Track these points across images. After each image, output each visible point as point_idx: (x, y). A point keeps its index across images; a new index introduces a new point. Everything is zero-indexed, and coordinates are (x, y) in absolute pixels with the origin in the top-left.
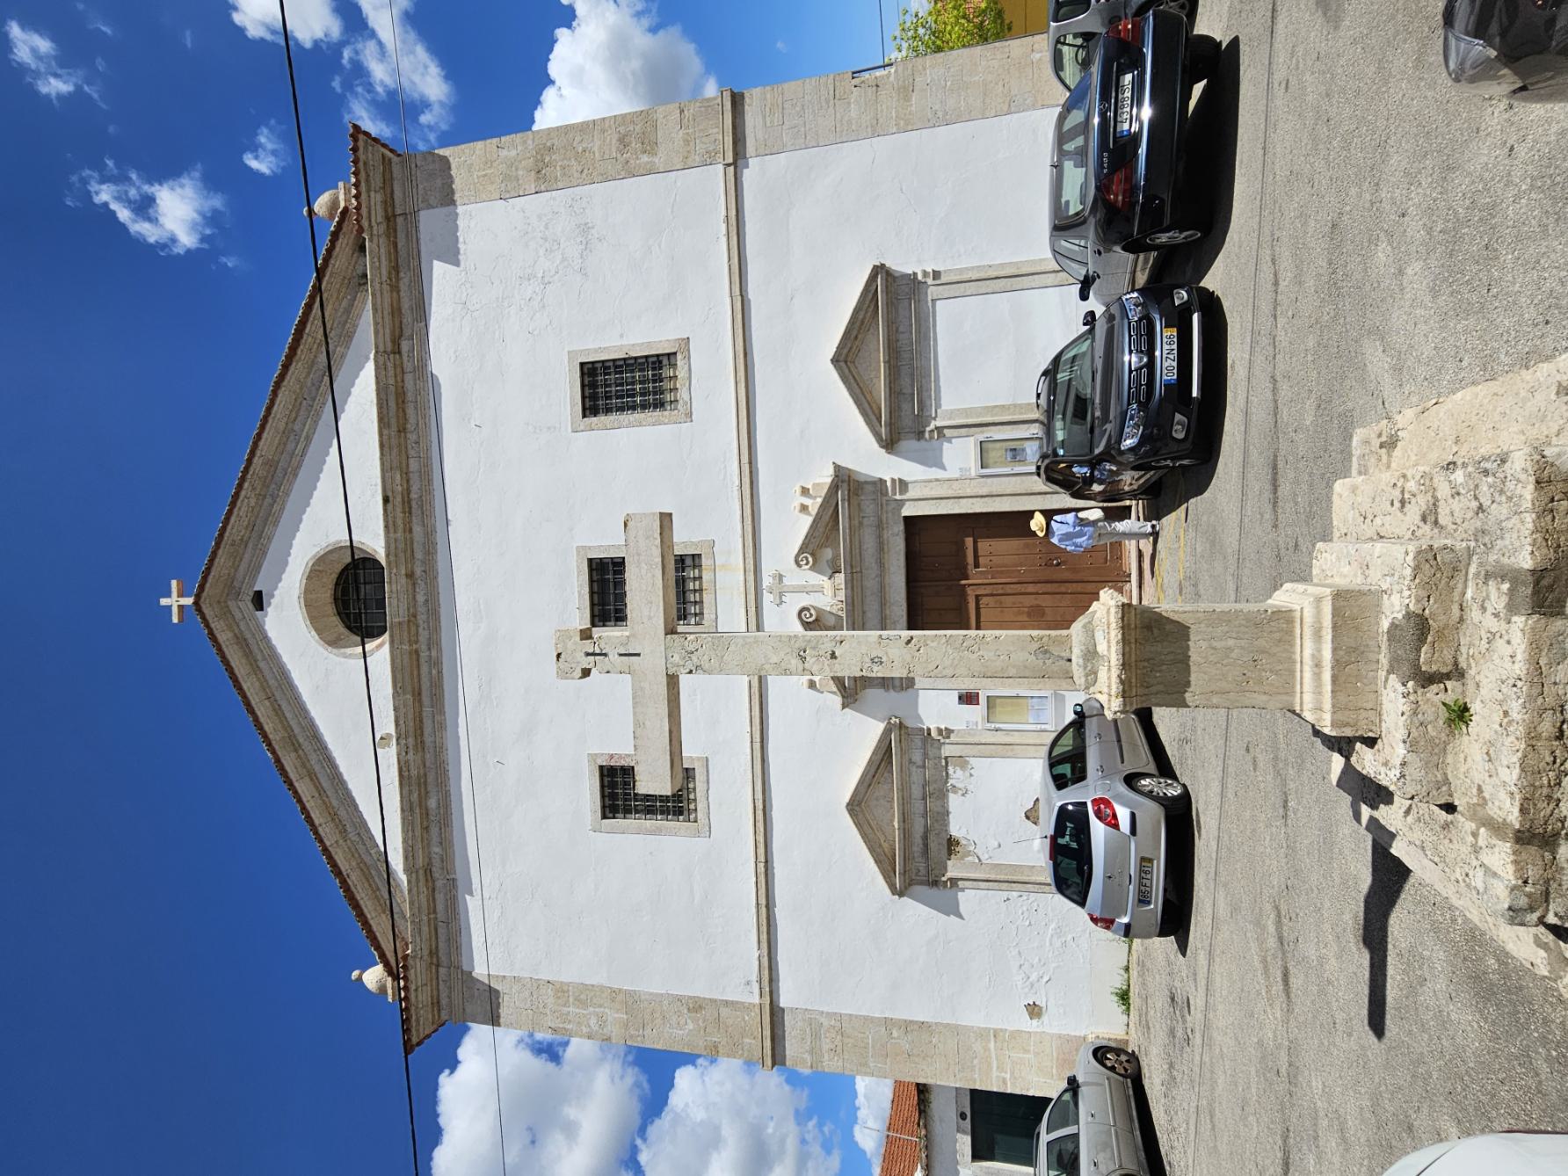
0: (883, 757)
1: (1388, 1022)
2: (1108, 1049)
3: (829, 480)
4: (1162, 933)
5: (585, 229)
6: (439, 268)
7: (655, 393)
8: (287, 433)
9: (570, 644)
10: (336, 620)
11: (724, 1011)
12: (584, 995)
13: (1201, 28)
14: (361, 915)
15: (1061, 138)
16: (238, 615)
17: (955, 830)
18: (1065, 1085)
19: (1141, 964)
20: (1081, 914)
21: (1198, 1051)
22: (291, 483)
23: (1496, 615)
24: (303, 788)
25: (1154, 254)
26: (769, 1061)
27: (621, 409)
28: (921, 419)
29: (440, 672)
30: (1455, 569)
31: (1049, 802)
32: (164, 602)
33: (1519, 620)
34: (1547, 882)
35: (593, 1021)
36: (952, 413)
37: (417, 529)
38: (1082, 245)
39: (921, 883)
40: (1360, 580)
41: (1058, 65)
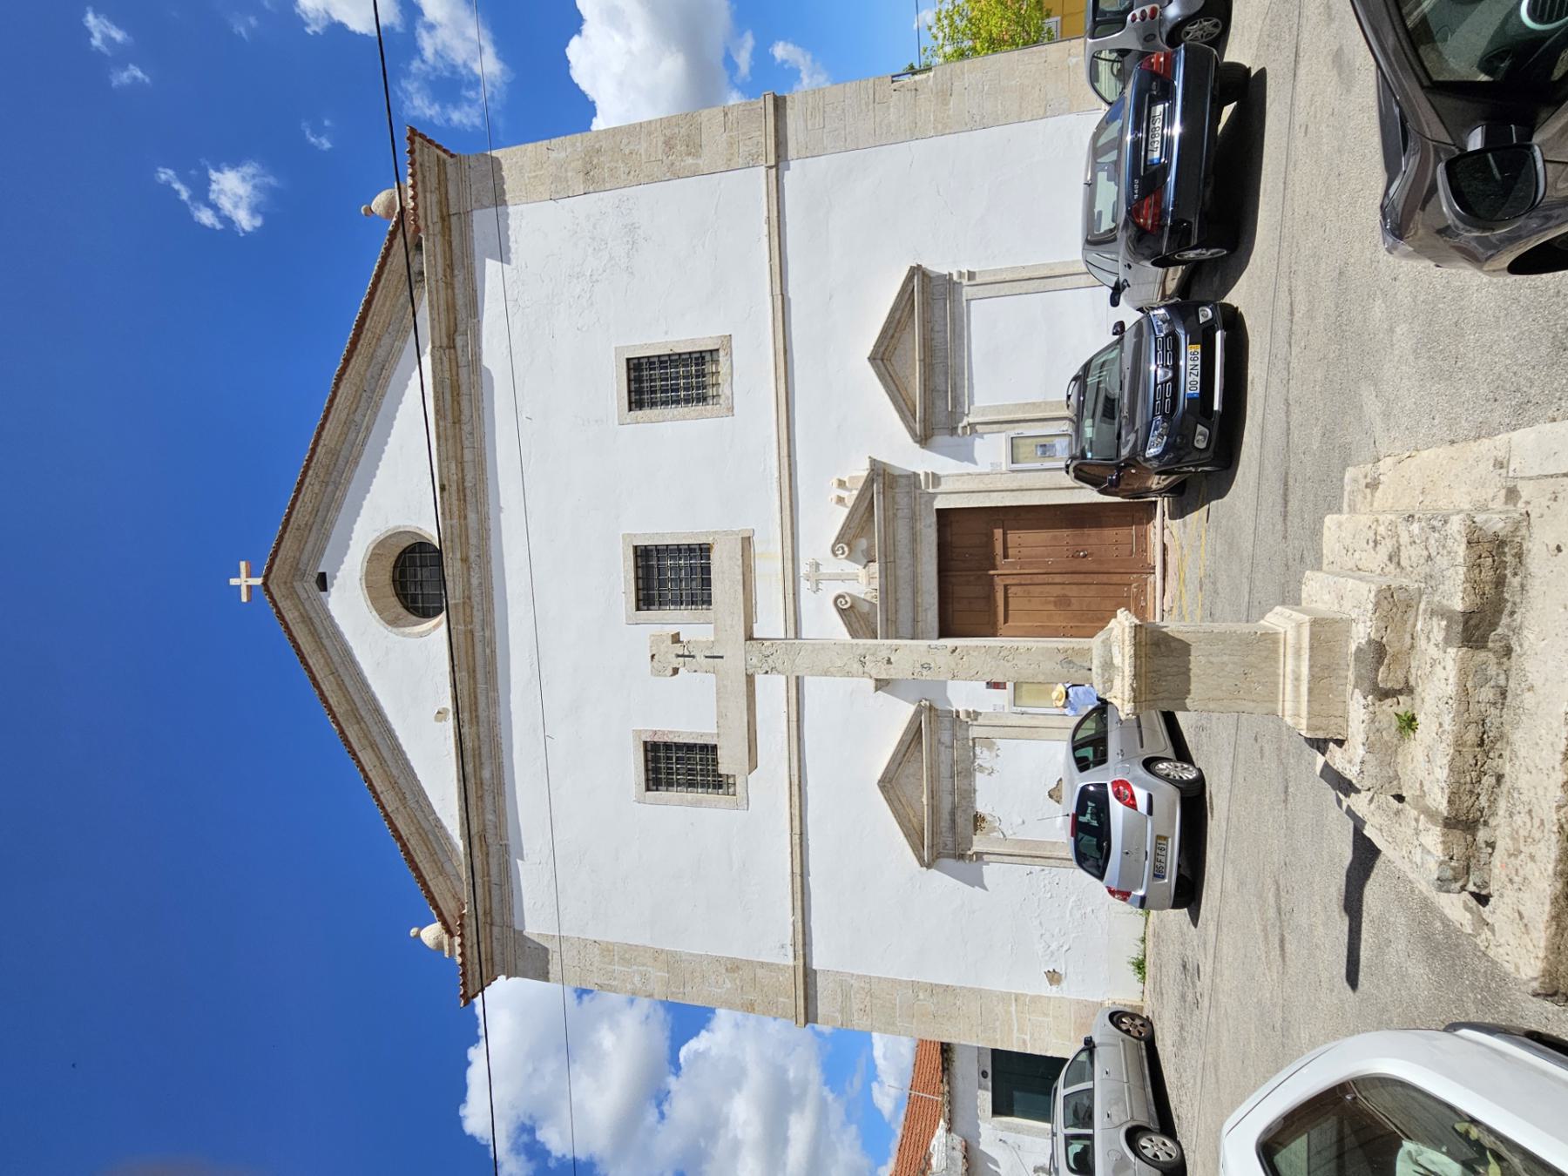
0: (913, 736)
1: (1361, 975)
2: (1125, 1014)
3: (865, 473)
4: (1176, 905)
5: (632, 228)
6: (492, 267)
7: (698, 388)
8: (349, 423)
9: (663, 648)
10: (394, 600)
11: (760, 972)
12: (627, 954)
13: (1231, 55)
14: (420, 876)
15: (1096, 152)
16: (304, 596)
17: (981, 807)
18: (1082, 1045)
19: (1157, 935)
20: (1099, 887)
21: (1205, 1013)
22: (353, 471)
23: (1437, 645)
24: (366, 757)
25: (1180, 268)
26: (802, 1019)
27: (665, 403)
28: (954, 416)
29: (493, 651)
30: (1408, 606)
31: (1071, 782)
32: (233, 582)
33: (1452, 651)
34: (1468, 858)
35: (637, 979)
36: (984, 410)
37: (472, 516)
38: (1116, 261)
39: (949, 856)
40: (1336, 608)
41: (1094, 77)
